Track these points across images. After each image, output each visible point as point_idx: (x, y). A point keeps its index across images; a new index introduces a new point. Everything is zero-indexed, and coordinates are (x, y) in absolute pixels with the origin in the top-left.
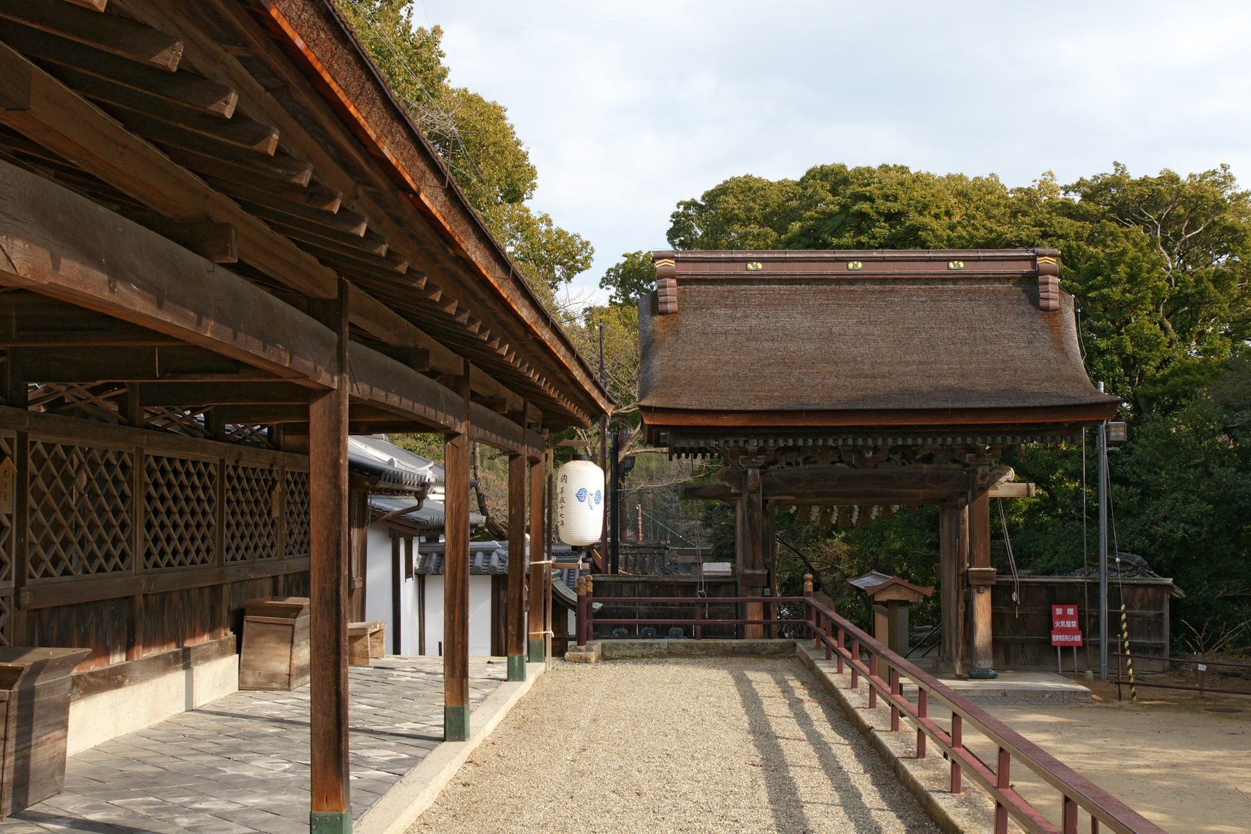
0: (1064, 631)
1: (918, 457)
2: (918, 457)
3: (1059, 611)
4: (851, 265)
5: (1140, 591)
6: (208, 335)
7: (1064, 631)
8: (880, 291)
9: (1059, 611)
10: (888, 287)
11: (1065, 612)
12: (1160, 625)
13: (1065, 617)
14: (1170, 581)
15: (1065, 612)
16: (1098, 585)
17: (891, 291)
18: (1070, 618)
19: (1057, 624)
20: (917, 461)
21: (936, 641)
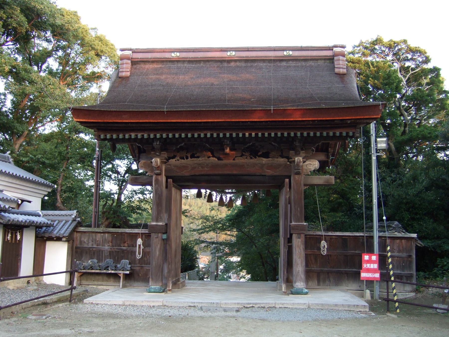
0: (368, 271)
1: (260, 153)
2: (260, 153)
3: (366, 257)
4: (229, 53)
5: (398, 241)
6: (19, 46)
7: (368, 271)
8: (295, 67)
9: (366, 257)
10: (249, 64)
11: (370, 258)
12: (411, 262)
13: (370, 261)
14: (415, 235)
15: (370, 258)
16: (372, 237)
17: (251, 66)
18: (373, 262)
19: (365, 266)
20: (259, 156)
21: (363, 297)
